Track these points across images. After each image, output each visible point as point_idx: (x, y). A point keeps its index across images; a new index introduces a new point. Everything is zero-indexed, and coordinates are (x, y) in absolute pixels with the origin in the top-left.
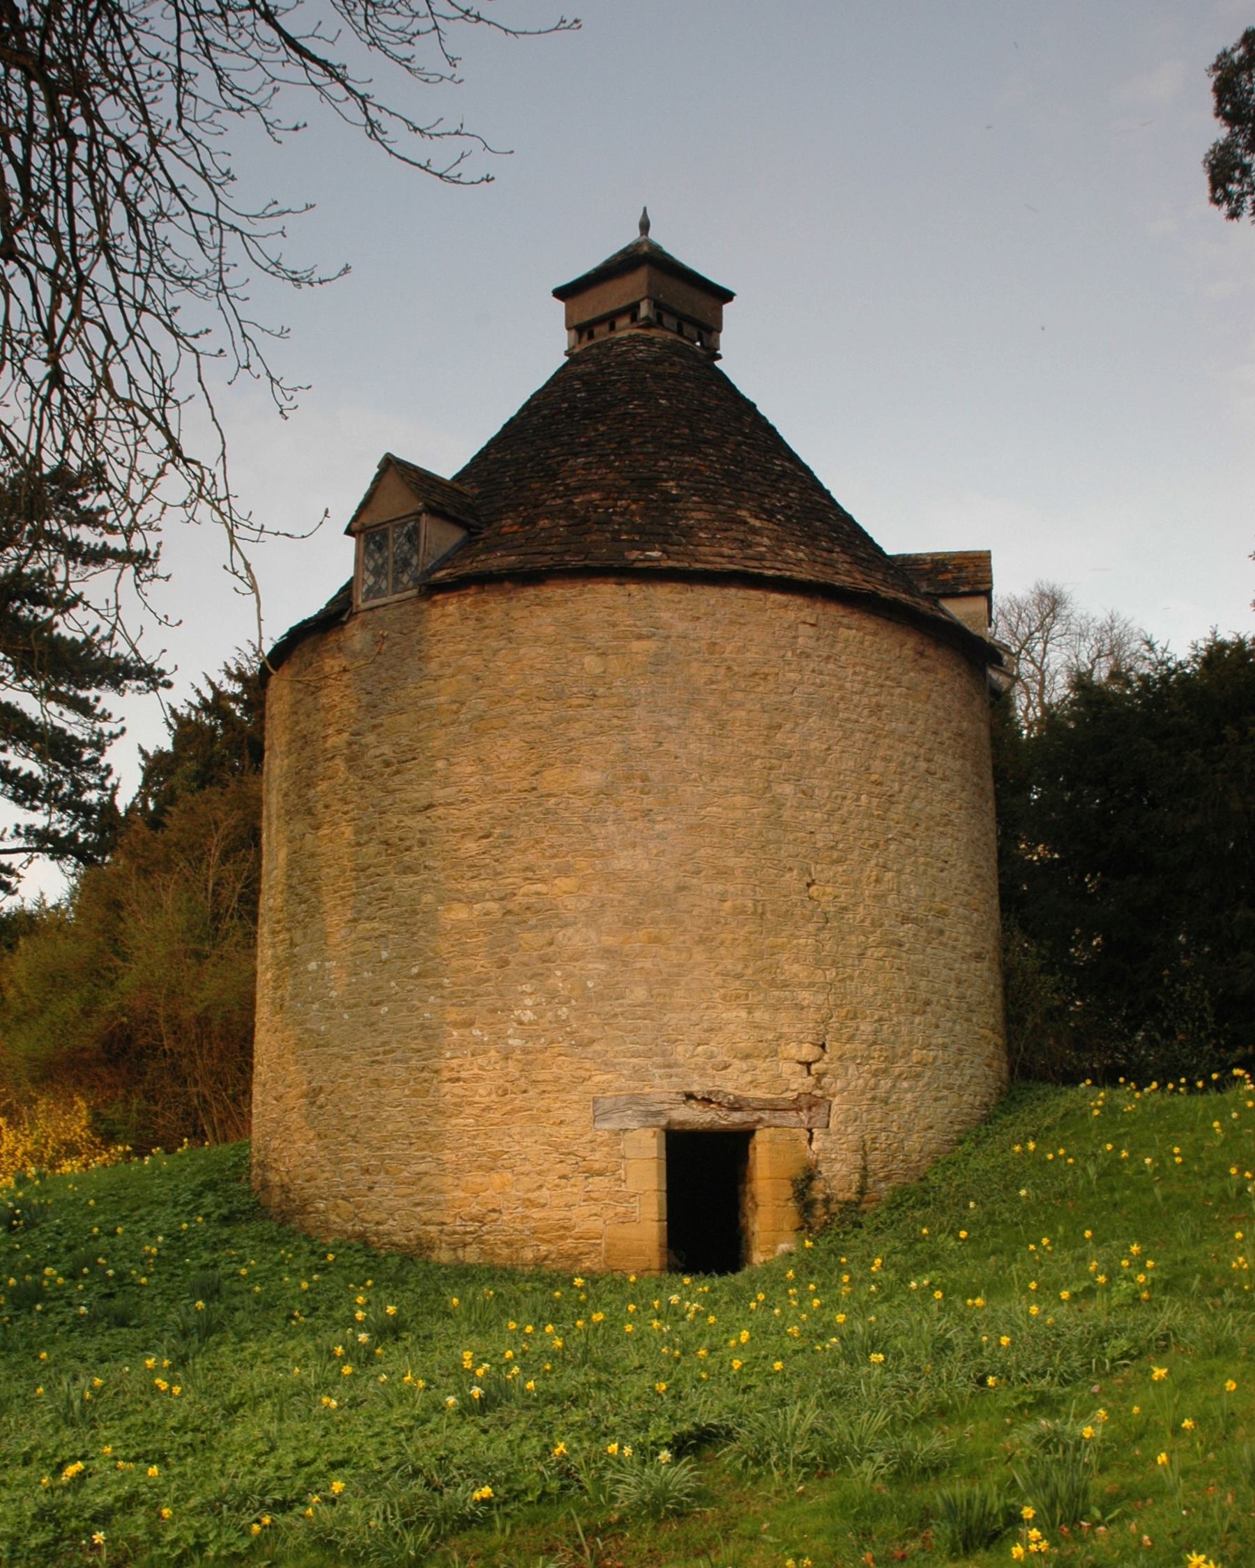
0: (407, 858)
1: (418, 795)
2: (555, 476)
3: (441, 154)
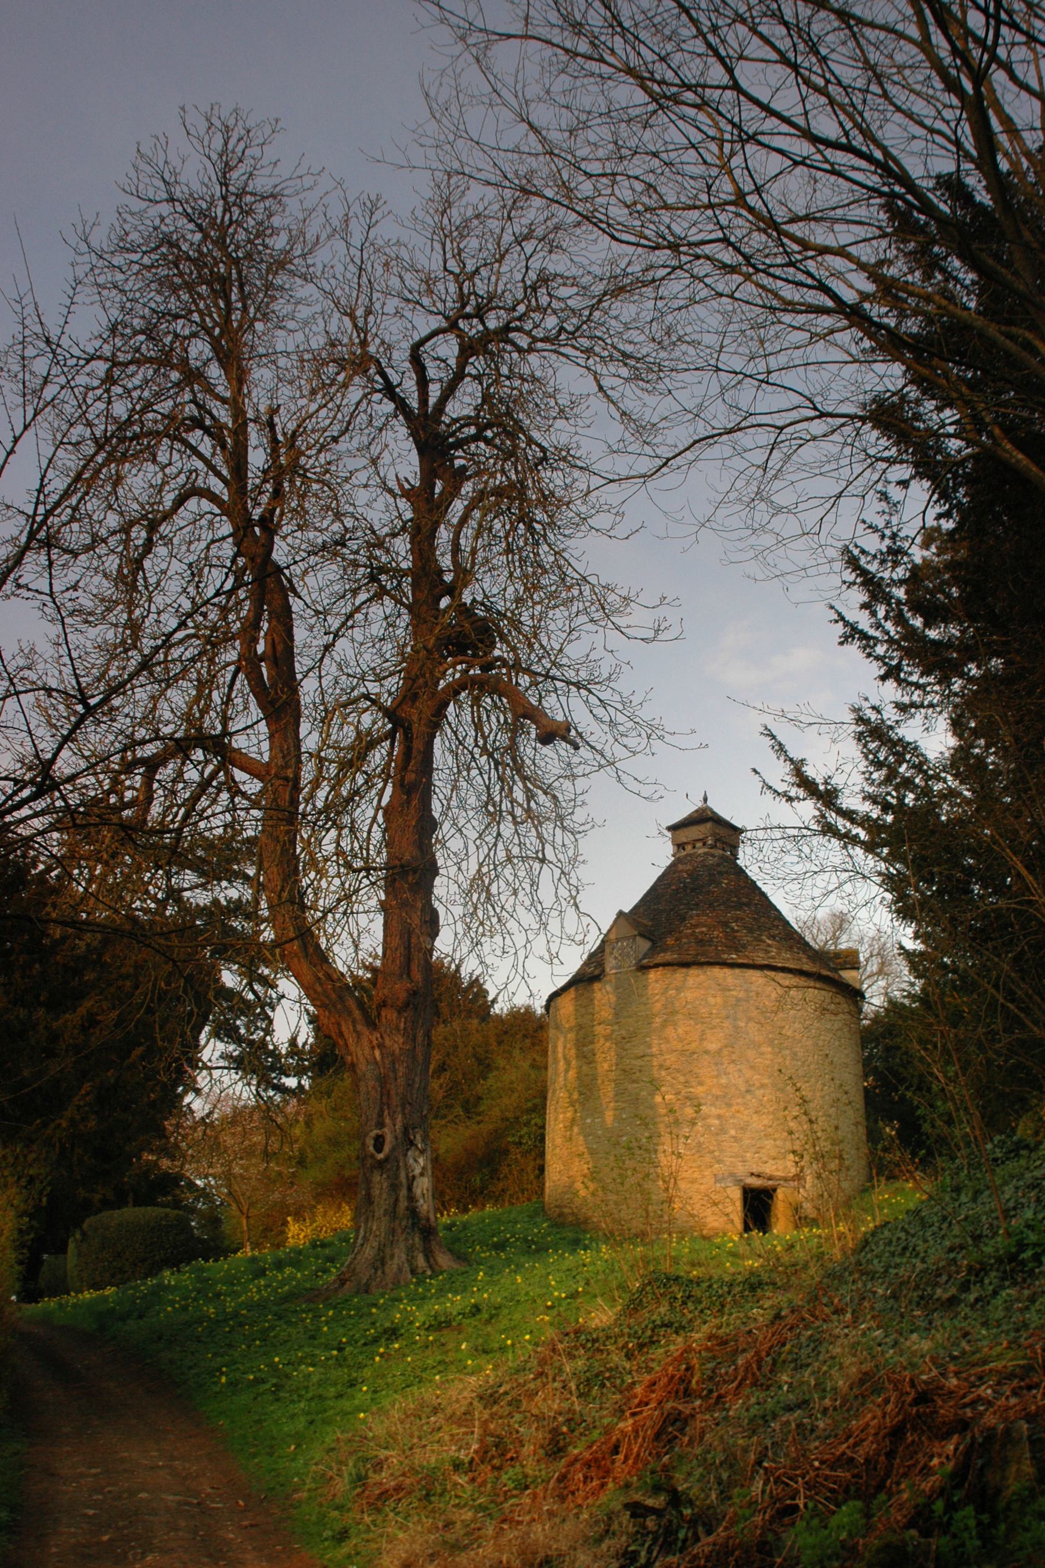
0: (634, 1077)
1: (640, 1050)
2: (684, 919)
3: (646, 791)
